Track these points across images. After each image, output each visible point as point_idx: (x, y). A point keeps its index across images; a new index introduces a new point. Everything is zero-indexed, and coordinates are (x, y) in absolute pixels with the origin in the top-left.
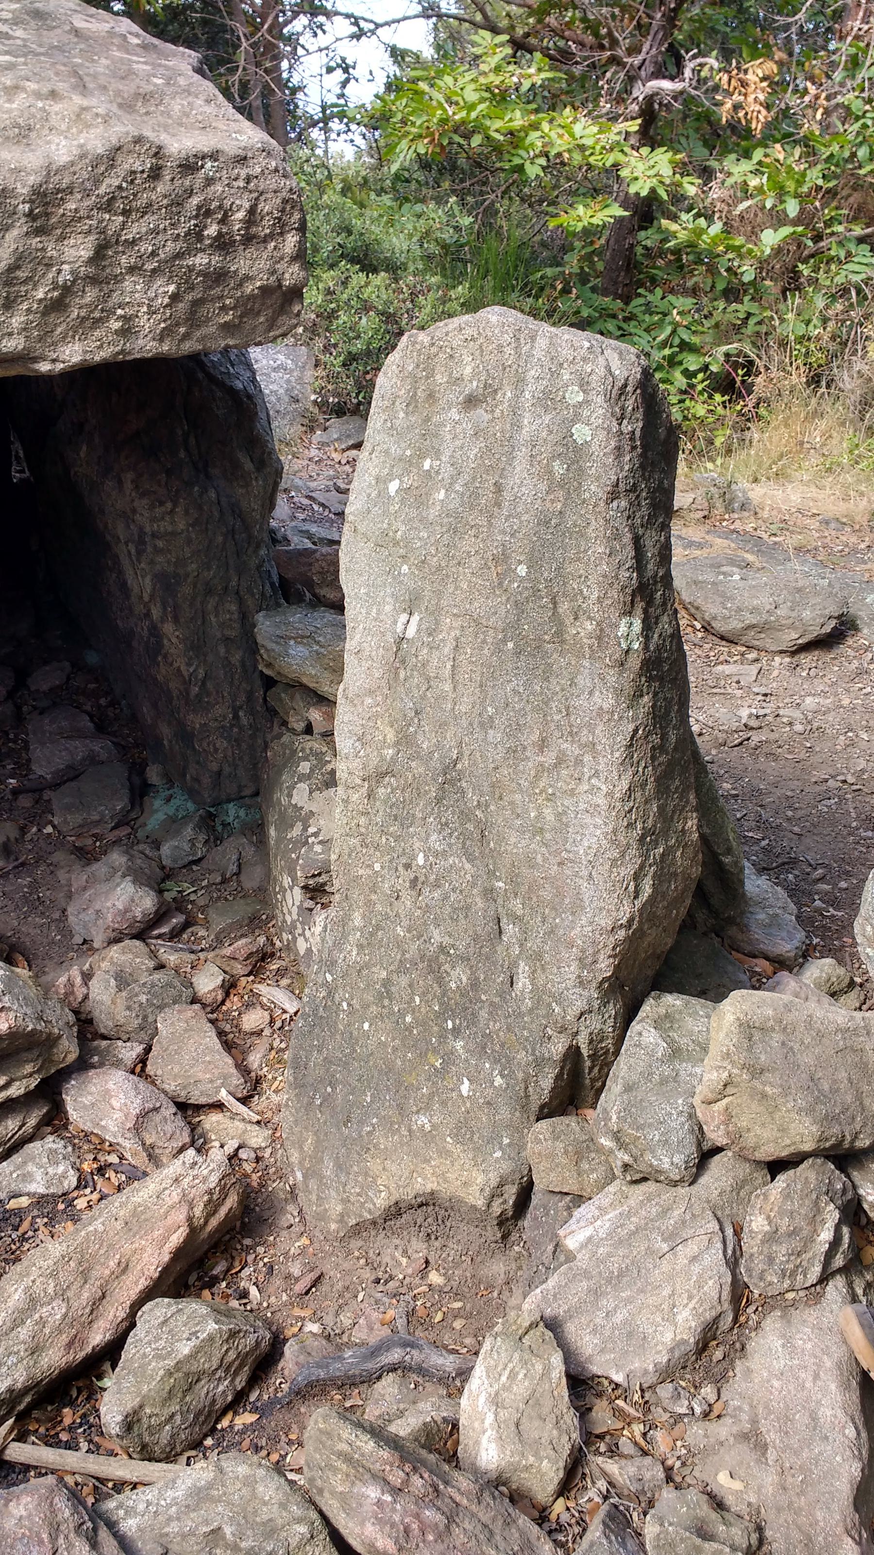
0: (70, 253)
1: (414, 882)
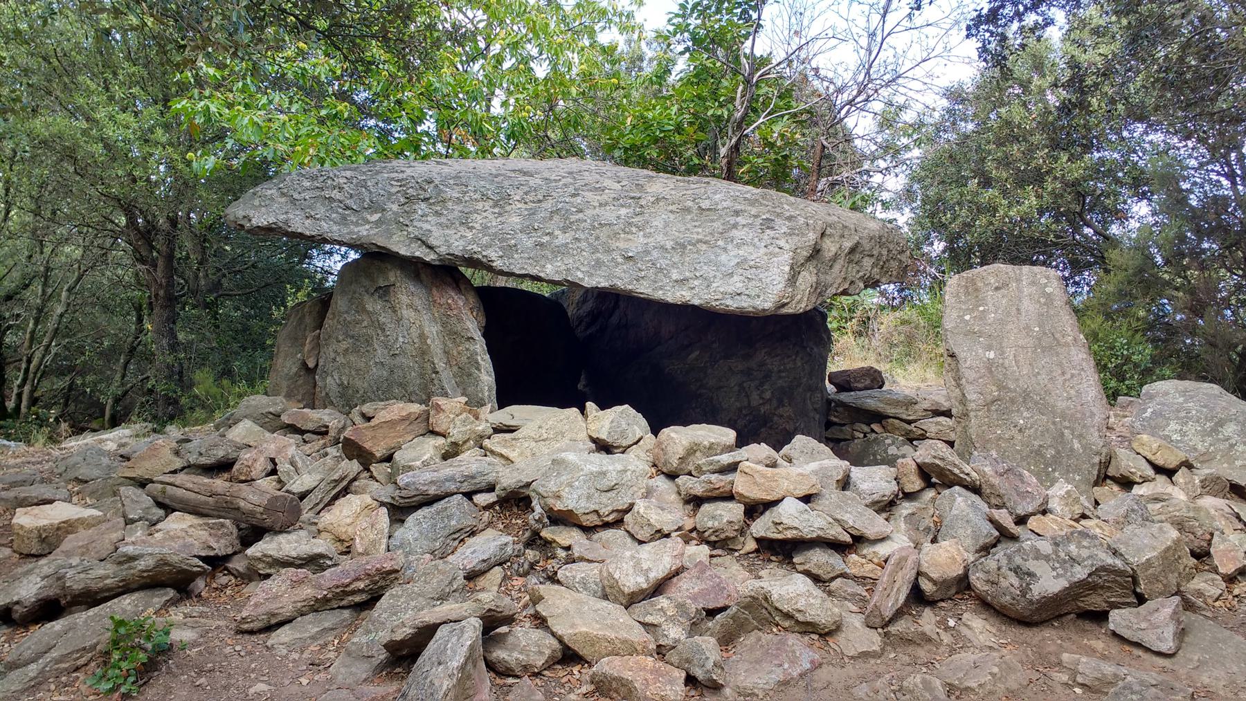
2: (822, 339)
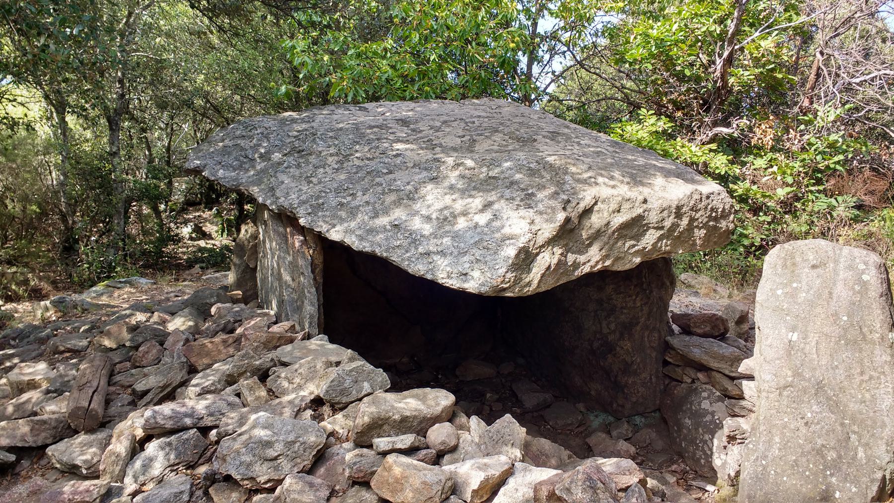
0: (683, 223)
1: (806, 424)
2: (663, 284)
